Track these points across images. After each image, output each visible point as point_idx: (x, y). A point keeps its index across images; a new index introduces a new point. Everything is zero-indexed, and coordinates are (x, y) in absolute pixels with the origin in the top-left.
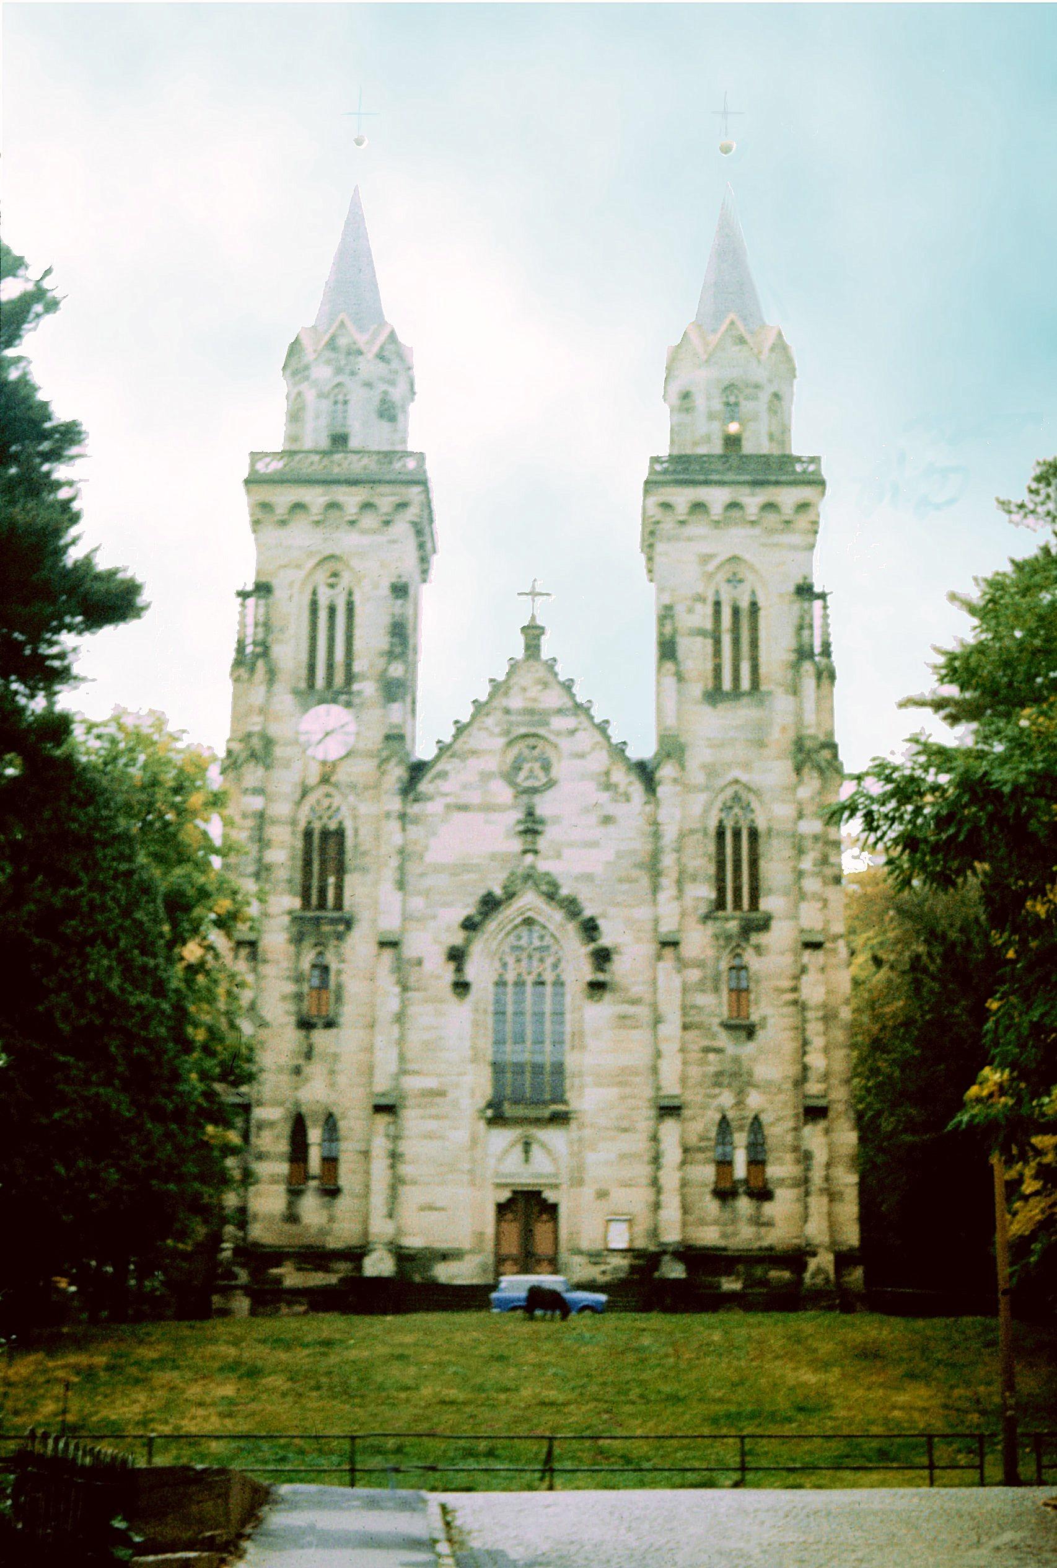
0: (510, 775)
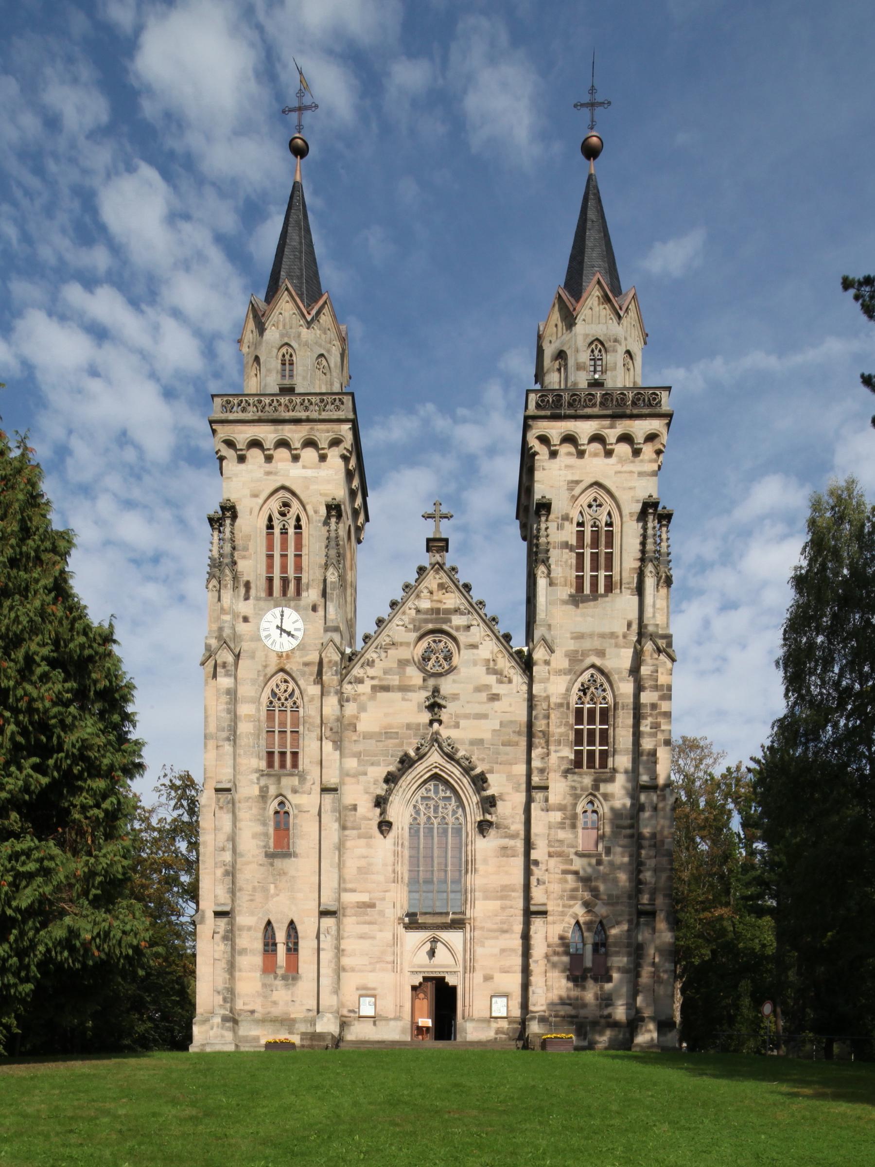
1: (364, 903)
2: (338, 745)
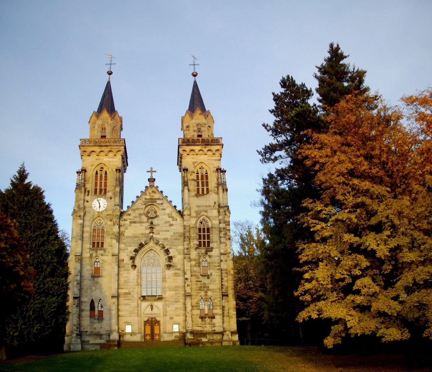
0: (146, 215)
1: (127, 293)
2: (119, 241)
